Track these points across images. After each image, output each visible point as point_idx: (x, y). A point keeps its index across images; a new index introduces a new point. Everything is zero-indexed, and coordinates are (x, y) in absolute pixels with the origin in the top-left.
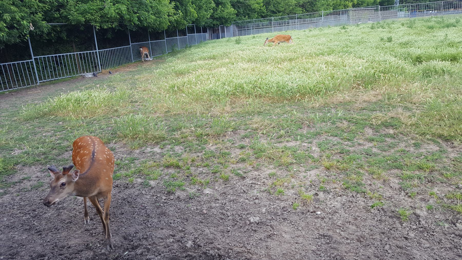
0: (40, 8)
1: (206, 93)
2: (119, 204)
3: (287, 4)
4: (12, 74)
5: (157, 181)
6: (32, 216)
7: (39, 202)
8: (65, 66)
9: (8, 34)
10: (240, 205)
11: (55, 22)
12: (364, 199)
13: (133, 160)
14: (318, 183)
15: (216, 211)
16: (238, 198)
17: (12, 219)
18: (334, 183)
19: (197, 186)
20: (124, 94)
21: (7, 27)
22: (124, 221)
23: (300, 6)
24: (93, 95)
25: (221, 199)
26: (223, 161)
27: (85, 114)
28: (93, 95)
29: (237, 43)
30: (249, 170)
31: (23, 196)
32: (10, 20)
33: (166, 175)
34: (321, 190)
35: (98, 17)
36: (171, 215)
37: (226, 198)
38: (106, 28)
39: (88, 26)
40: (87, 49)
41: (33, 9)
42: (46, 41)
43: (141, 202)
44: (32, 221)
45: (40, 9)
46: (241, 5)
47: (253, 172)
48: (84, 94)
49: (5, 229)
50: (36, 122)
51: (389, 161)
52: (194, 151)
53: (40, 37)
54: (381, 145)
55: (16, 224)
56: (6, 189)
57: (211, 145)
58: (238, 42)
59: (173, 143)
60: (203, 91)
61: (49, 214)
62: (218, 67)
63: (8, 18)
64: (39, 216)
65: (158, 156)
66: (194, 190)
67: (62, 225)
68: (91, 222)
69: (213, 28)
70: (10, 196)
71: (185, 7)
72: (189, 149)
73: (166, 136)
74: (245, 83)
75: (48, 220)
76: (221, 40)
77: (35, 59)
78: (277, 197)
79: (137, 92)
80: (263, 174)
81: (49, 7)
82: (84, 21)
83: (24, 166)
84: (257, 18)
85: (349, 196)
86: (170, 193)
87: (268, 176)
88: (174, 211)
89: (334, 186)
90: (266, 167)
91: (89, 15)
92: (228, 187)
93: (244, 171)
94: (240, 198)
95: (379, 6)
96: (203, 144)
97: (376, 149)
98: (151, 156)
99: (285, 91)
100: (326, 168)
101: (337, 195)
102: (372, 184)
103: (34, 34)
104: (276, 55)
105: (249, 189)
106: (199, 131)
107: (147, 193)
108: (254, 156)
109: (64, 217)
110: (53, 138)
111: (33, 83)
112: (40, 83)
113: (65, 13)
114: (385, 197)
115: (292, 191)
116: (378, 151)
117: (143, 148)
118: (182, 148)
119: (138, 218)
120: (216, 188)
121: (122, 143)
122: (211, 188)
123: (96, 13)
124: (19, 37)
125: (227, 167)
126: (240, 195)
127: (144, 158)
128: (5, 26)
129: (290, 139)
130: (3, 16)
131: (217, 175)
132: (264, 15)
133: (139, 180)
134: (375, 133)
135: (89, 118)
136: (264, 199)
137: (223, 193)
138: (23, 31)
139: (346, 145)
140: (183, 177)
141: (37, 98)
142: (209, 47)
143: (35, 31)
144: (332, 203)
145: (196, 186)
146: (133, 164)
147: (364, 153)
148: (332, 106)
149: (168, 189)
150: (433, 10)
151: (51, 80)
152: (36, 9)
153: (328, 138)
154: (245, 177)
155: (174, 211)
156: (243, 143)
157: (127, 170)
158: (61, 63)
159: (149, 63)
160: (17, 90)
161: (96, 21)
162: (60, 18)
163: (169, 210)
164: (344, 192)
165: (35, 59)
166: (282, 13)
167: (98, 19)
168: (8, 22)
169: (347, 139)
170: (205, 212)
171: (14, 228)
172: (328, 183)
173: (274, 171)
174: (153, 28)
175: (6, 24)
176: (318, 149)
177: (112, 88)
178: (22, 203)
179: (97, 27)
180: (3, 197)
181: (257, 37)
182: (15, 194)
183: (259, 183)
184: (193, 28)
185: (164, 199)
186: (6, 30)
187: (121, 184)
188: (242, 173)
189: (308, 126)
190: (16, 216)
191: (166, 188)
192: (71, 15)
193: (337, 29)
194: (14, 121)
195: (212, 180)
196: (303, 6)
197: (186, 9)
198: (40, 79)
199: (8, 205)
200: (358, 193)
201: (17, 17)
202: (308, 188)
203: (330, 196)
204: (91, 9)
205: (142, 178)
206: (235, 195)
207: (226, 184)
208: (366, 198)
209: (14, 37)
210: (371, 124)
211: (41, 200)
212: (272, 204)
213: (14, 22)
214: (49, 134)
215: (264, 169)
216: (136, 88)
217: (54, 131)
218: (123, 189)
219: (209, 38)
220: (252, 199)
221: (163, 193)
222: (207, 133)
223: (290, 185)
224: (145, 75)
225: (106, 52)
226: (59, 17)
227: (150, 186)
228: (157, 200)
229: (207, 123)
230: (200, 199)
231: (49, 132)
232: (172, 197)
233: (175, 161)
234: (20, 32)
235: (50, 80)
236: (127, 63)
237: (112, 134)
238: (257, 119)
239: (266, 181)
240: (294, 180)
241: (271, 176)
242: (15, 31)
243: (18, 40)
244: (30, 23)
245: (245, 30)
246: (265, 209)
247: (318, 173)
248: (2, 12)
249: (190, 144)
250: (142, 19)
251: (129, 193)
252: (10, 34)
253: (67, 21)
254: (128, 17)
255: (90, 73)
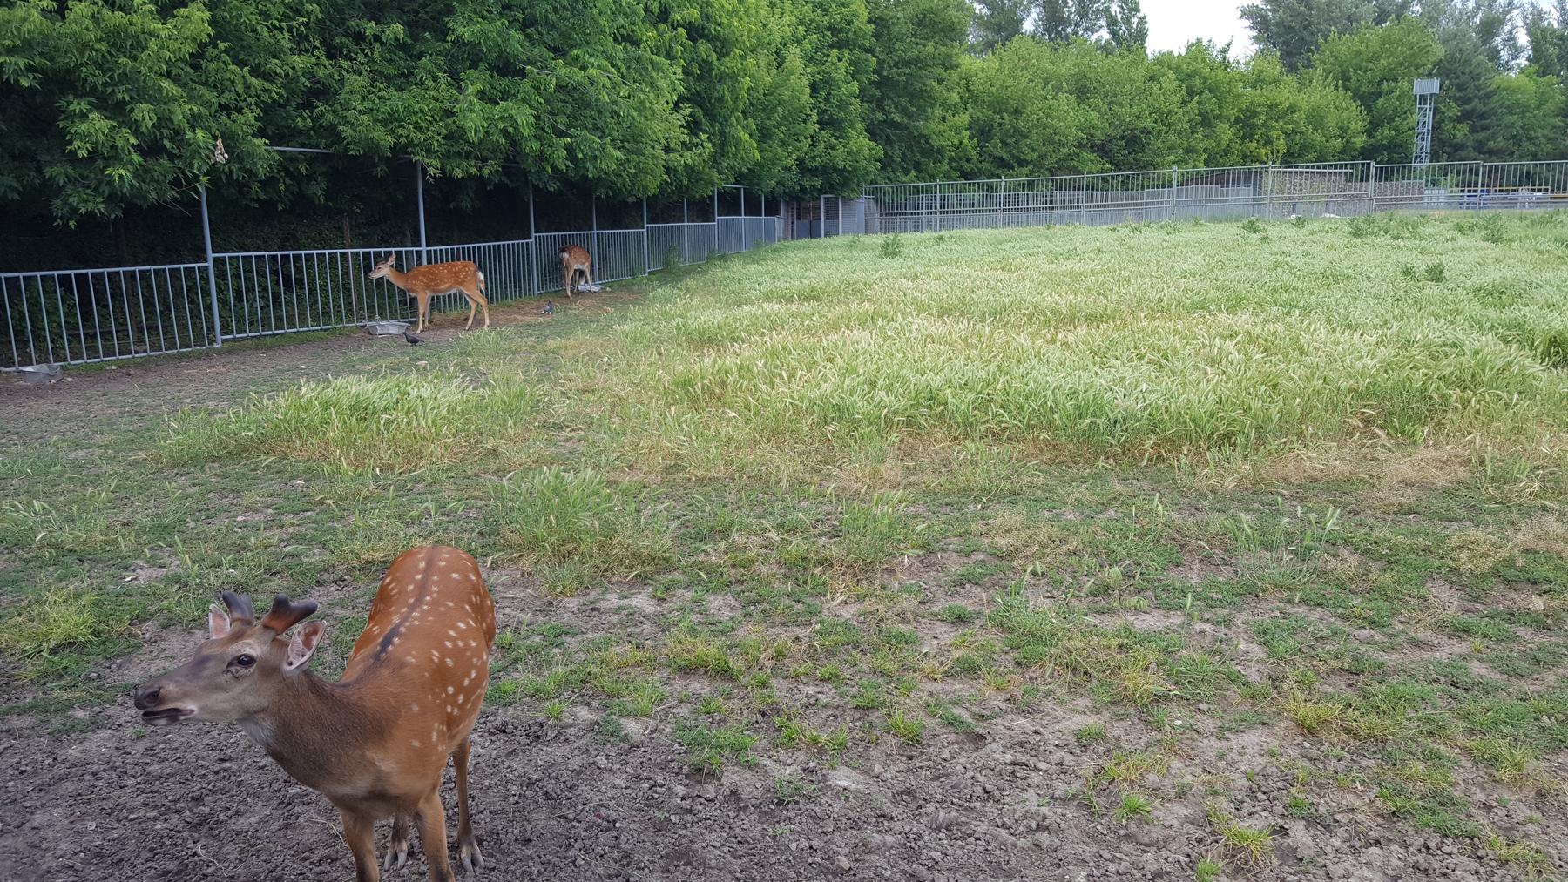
0: (253, 94)
1: (807, 411)
2: (512, 800)
3: (1049, 141)
4: (134, 306)
5: (652, 723)
6: (188, 820)
7: (216, 769)
8: (312, 292)
9: (140, 172)
10: (981, 849)
11: (294, 143)
12: (1475, 865)
13: (559, 635)
14: (1280, 784)
15: (886, 866)
16: (965, 819)
17: (116, 825)
18: (1341, 788)
19: (800, 755)
20: (521, 396)
21: (138, 148)
22: (535, 870)
23: (1092, 147)
24: (414, 394)
25: (900, 818)
26: (889, 666)
27: (386, 455)
28: (414, 394)
29: (887, 255)
30: (997, 710)
31: (158, 738)
32: (153, 125)
33: (681, 701)
34: (1298, 812)
35: (439, 138)
36: (713, 863)
37: (920, 814)
38: (460, 176)
39: (401, 163)
40: (386, 242)
41: (229, 97)
42: (257, 206)
43: (595, 801)
44: (190, 841)
45: (250, 96)
46: (895, 135)
47: (1009, 717)
48: (382, 389)
49: (88, 864)
50: (210, 474)
51: (1545, 717)
52: (778, 620)
53: (240, 192)
54: (1498, 650)
55: (131, 845)
56: (97, 709)
57: (840, 599)
58: (890, 251)
59: (701, 581)
60: (797, 402)
61: (253, 820)
62: (835, 327)
63: (147, 118)
64: (216, 822)
65: (647, 626)
66: (794, 767)
67: (299, 868)
68: (410, 862)
69: (799, 200)
70: (113, 736)
71: (721, 124)
72: (757, 604)
73: (674, 557)
74: (949, 387)
75: (250, 842)
76: (824, 241)
77: (215, 260)
78: (1122, 826)
79: (563, 393)
80: (1050, 728)
81: (282, 91)
82: (390, 148)
83: (165, 627)
84: (947, 176)
85: (1412, 845)
86: (699, 774)
87: (1072, 740)
88: (726, 849)
89: (1344, 802)
90: (1062, 702)
91: (411, 126)
92: (921, 767)
93: (977, 709)
94: (975, 818)
95: (1373, 164)
96: (812, 595)
97: (1484, 665)
98: (624, 624)
99: (1102, 421)
100: (1301, 725)
101: (1362, 837)
102: (1495, 804)
103: (223, 177)
104: (1038, 298)
105: (1007, 787)
106: (797, 545)
107: (616, 767)
108: (1008, 657)
109: (306, 837)
110: (273, 537)
111: (199, 340)
112: (224, 341)
113: (330, 117)
114: (1558, 863)
115: (1181, 810)
116: (1492, 675)
117: (593, 594)
118: (733, 602)
119: (586, 862)
120: (878, 769)
121: (518, 570)
122: (854, 769)
123: (431, 123)
124: (175, 183)
125: (910, 690)
126: (972, 805)
127: (596, 628)
128: (133, 145)
129: (1144, 604)
130: (132, 110)
131: (874, 717)
132: (968, 167)
133: (584, 713)
134: (1469, 605)
135: (397, 471)
136: (1069, 832)
137: (902, 793)
138: (191, 165)
139: (1365, 643)
140: (745, 712)
141: (213, 390)
142: (789, 260)
143: (227, 169)
144: (1351, 869)
145: (798, 754)
146: (557, 650)
147: (1443, 679)
148: (1285, 492)
149: (693, 759)
150: (1547, 190)
151: (261, 336)
152: (238, 95)
153: (1289, 608)
154: (982, 737)
155: (726, 849)
156: (962, 603)
157: (538, 669)
158: (300, 282)
159: (588, 302)
160: (147, 360)
161: (429, 151)
162: (312, 133)
163: (704, 841)
164: (1391, 831)
165: (215, 260)
166: (1030, 167)
167: (435, 143)
168: (145, 131)
169: (1364, 619)
170: (845, 863)
171: (120, 865)
172: (1319, 787)
173: (1093, 722)
174: (610, 188)
175: (137, 138)
176: (1257, 651)
177: (477, 377)
178: (152, 768)
179: (432, 171)
180: (84, 740)
181: (951, 237)
182: (130, 731)
183: (1043, 766)
184: (735, 195)
185: (680, 794)
186: (136, 158)
187: (517, 723)
188: (970, 720)
189: (1207, 560)
190: (131, 816)
191: (685, 752)
192: (348, 122)
193: (1229, 231)
194: (135, 463)
195: (857, 734)
196: (1102, 150)
197: (722, 133)
198: (226, 329)
199: (104, 771)
200: (1446, 836)
201: (178, 118)
202: (1242, 802)
203: (1336, 842)
204: (415, 113)
205: (595, 704)
206: (952, 803)
207: (910, 758)
208: (1480, 858)
209: (157, 181)
210: (1452, 570)
211: (223, 760)
212: (1107, 855)
213: (166, 132)
214: (256, 517)
215: (1054, 710)
216: (557, 378)
217: (277, 509)
218: (524, 741)
219: (784, 233)
220: (1021, 828)
221: (676, 770)
222: (826, 553)
223: (1166, 781)
224: (580, 340)
225: (509, 250)
226: (309, 130)
227: (626, 738)
228: (653, 798)
229: (819, 517)
230: (817, 809)
231: (256, 511)
232: (710, 790)
233: (712, 651)
234: (180, 168)
235: (257, 334)
236: (516, 296)
237: (480, 533)
238: (1004, 516)
239: (1070, 761)
240: (1181, 765)
241: (1085, 741)
242: (165, 161)
243: (170, 194)
244: (215, 138)
245: (906, 214)
246: (1084, 874)
247: (1274, 744)
248: (131, 98)
249: (764, 591)
250: (580, 156)
251: (547, 758)
252: (147, 171)
253: (333, 143)
254: (536, 146)
255: (393, 322)
